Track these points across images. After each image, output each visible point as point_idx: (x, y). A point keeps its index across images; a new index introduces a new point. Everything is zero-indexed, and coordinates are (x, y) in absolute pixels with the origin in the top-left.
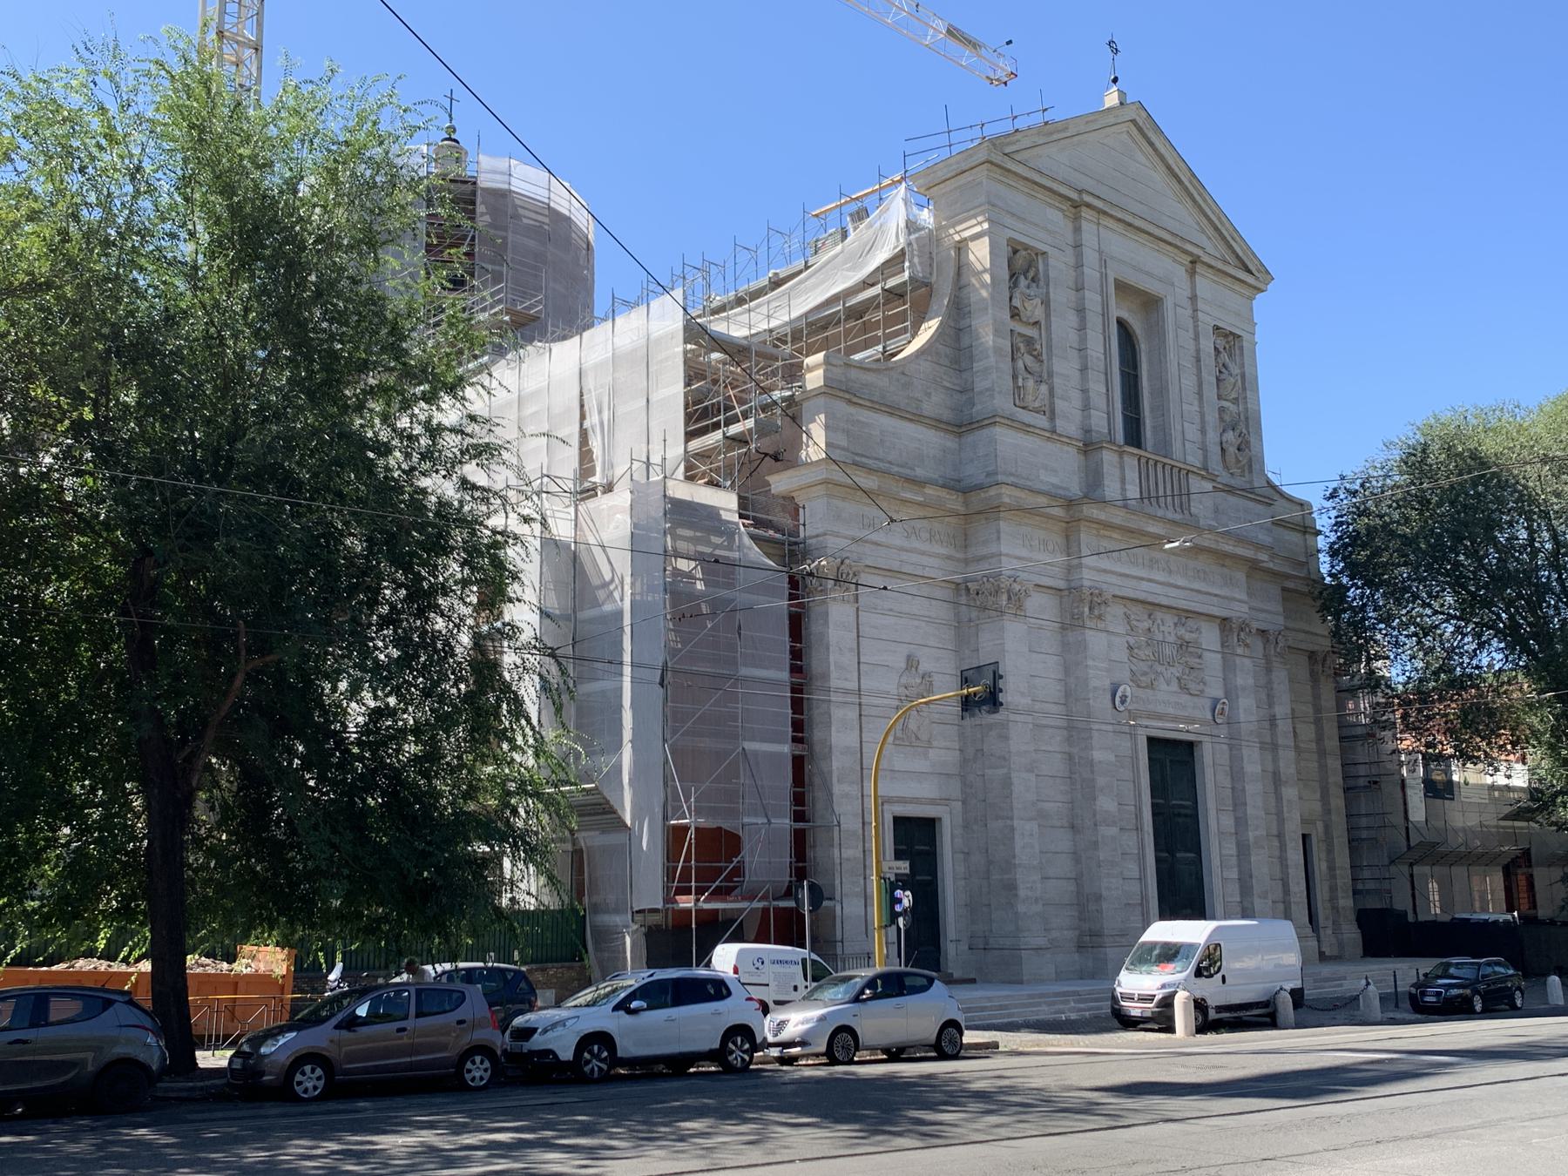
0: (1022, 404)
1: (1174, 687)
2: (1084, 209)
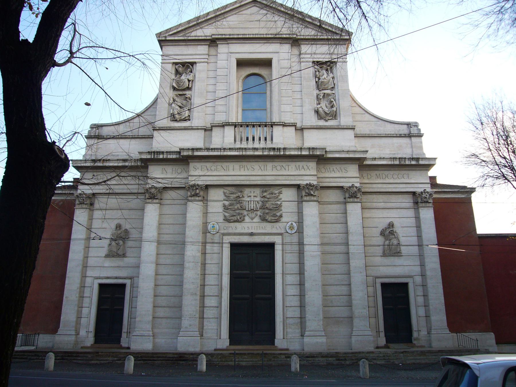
0: (175, 120)
1: (257, 219)
2: (216, 40)
